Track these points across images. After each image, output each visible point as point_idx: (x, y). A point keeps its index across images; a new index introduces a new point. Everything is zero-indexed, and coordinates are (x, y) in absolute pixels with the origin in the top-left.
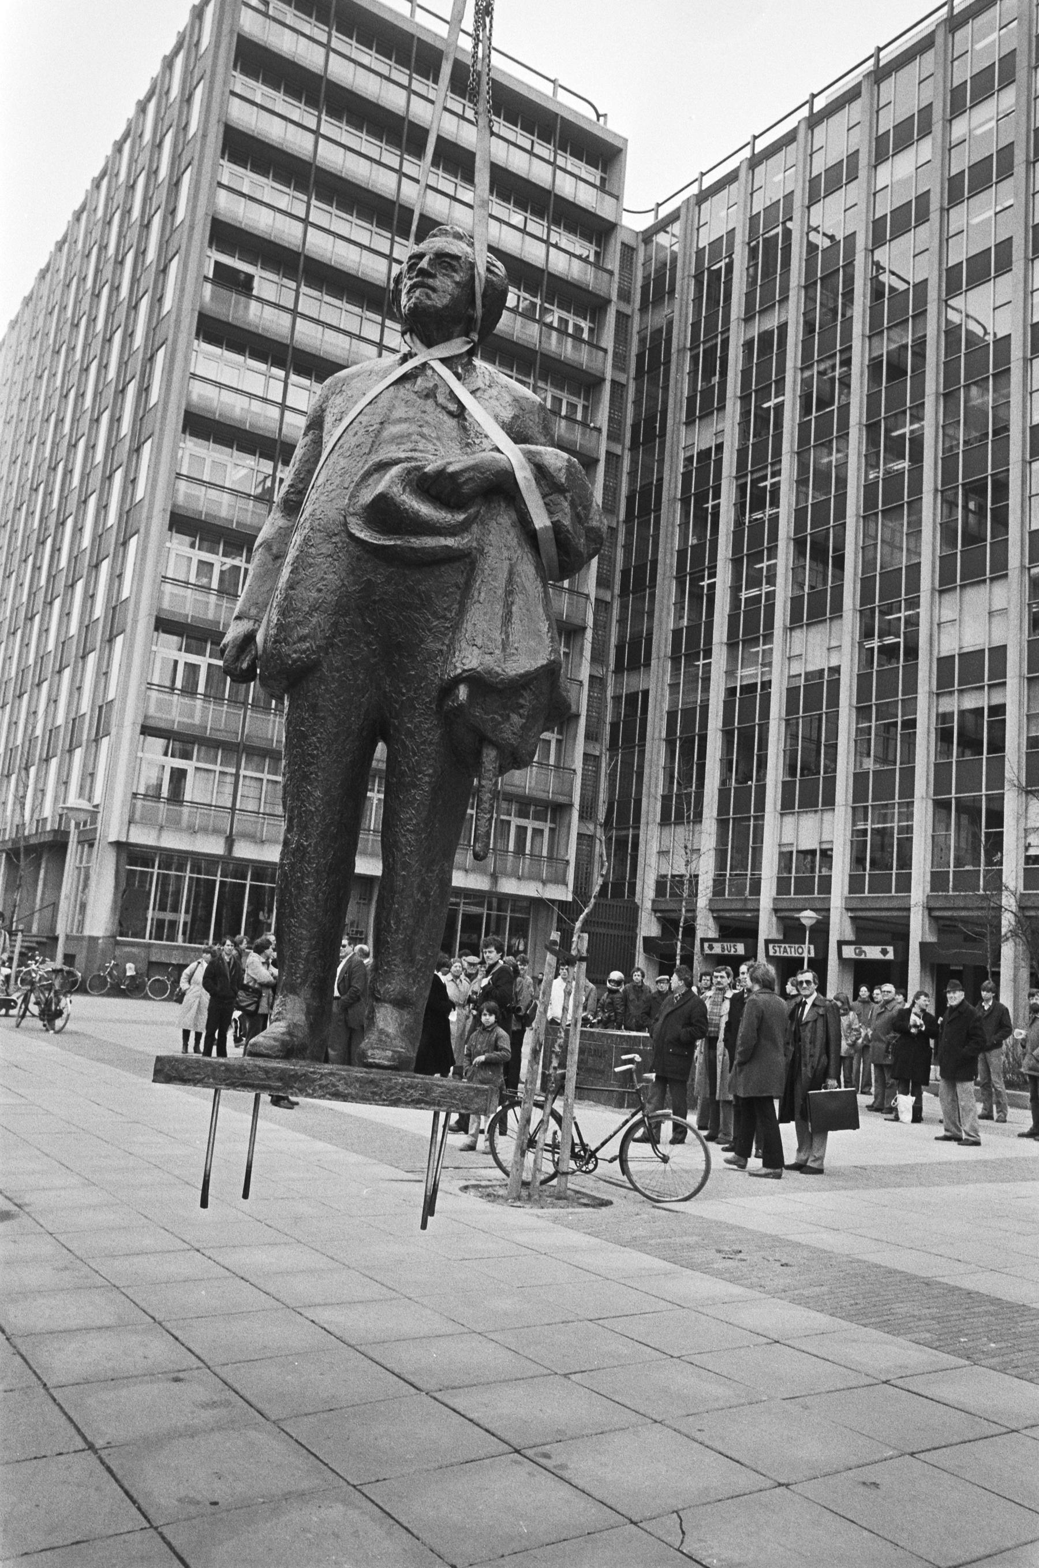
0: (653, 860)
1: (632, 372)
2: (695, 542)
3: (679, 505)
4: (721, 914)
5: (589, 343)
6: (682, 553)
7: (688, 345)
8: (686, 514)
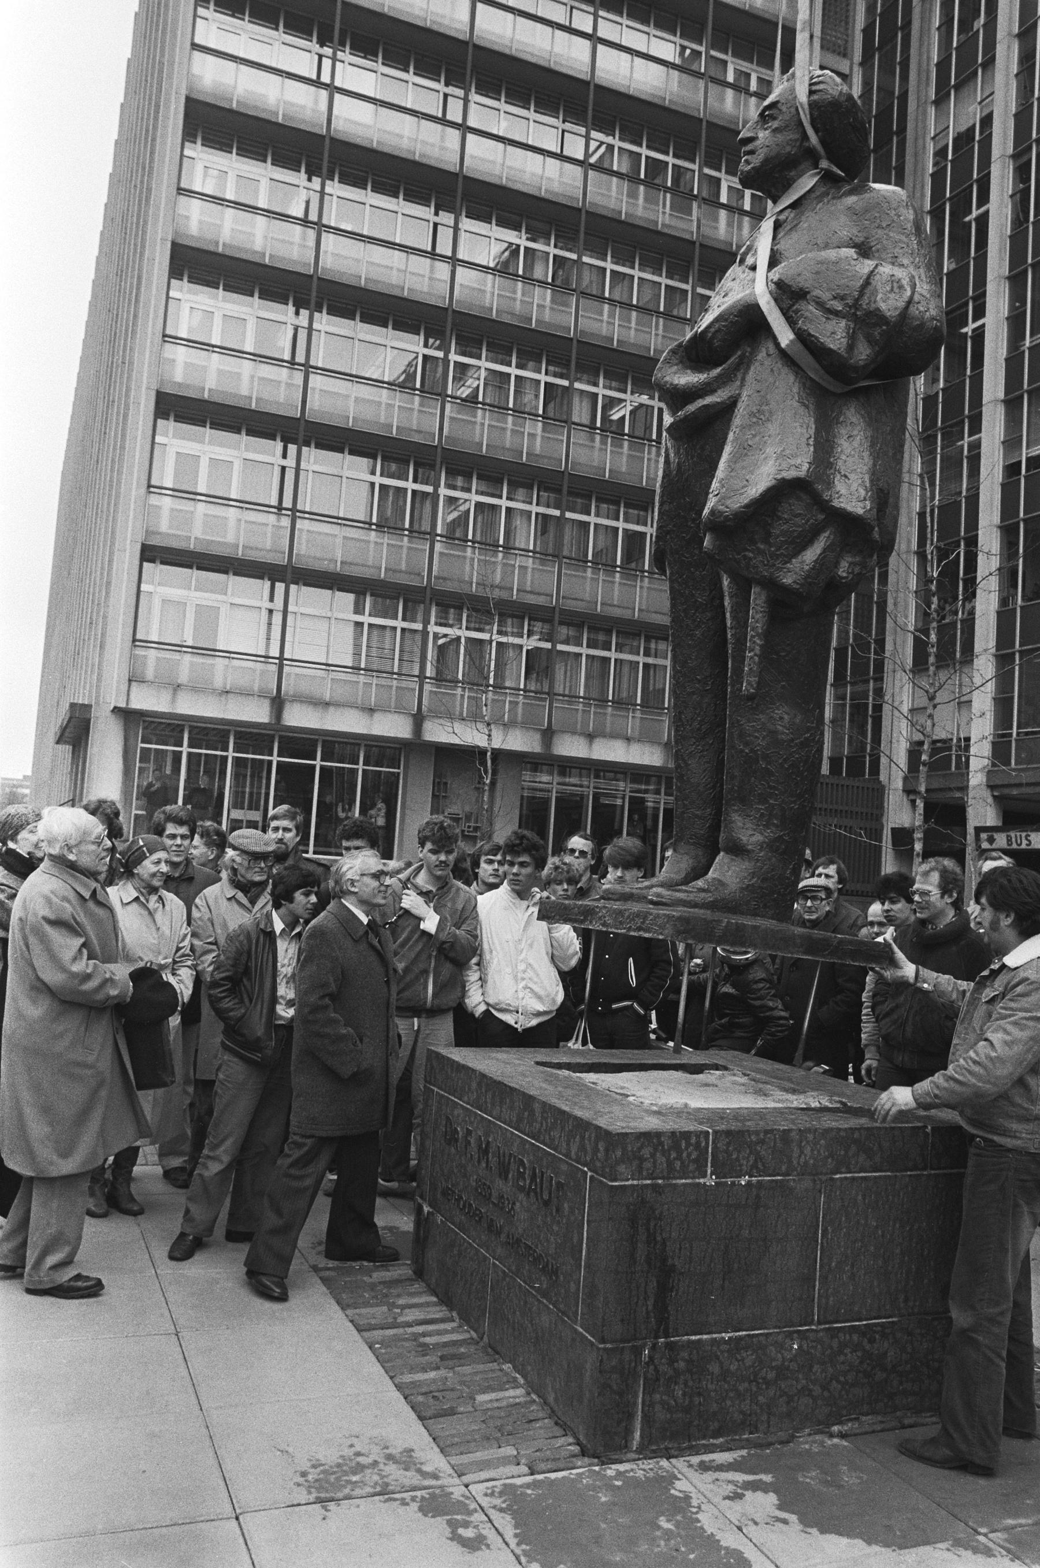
0: (903, 726)
2: (953, 266)
4: (1006, 791)
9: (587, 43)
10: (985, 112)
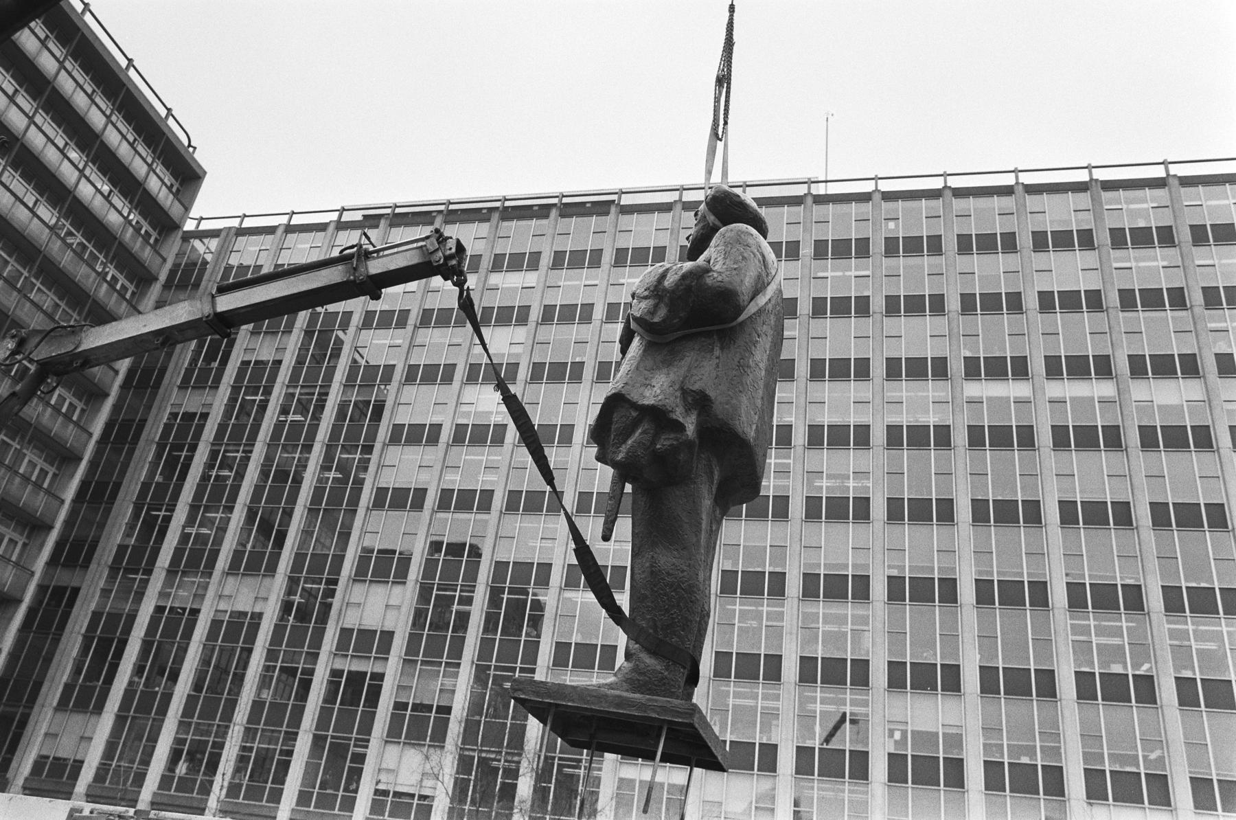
3: (154, 447)
6: (145, 486)
8: (158, 456)
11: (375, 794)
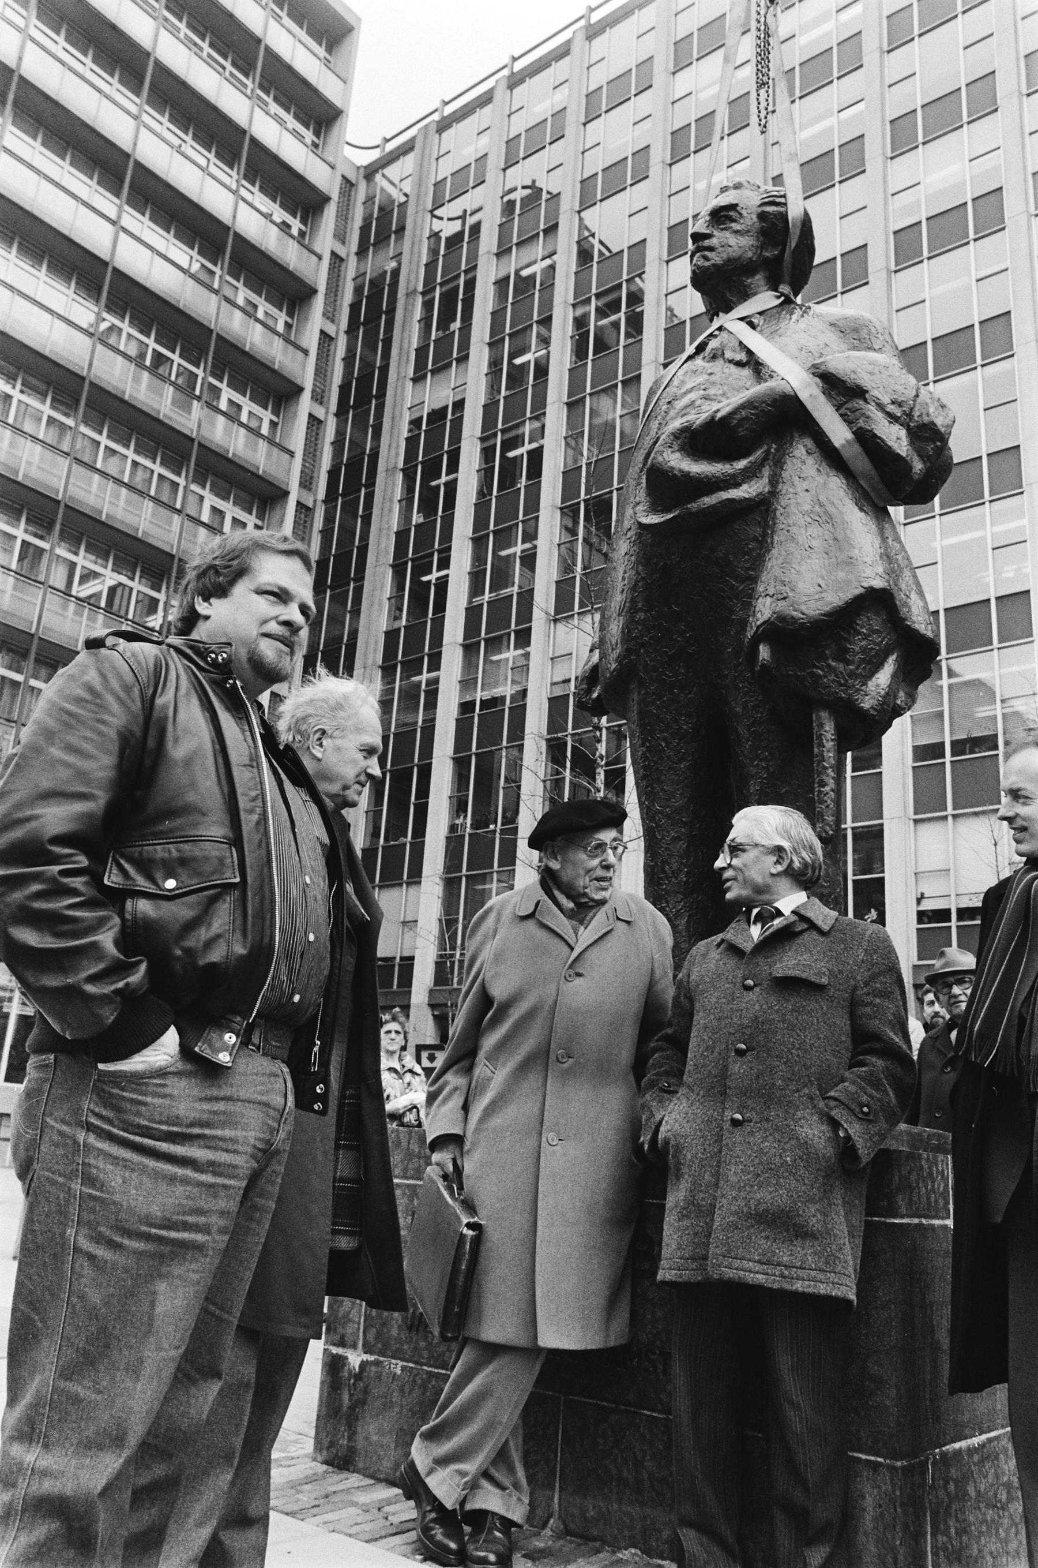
1: (333, 407)
2: (421, 520)
3: (400, 477)
5: (271, 441)
6: (402, 536)
7: (420, 289)
8: (409, 489)
9: (110, 227)
10: (457, 398)
11: (920, 921)
